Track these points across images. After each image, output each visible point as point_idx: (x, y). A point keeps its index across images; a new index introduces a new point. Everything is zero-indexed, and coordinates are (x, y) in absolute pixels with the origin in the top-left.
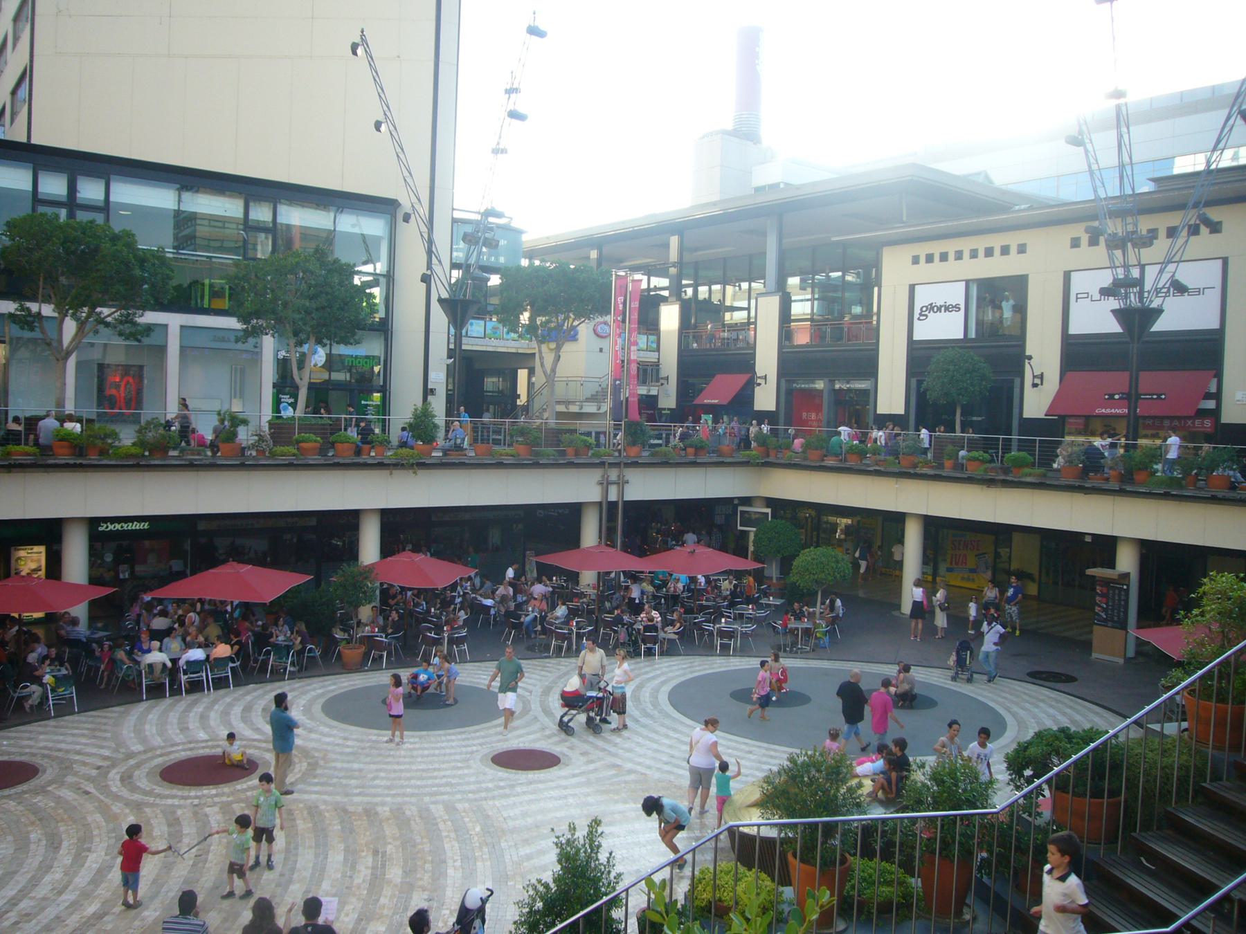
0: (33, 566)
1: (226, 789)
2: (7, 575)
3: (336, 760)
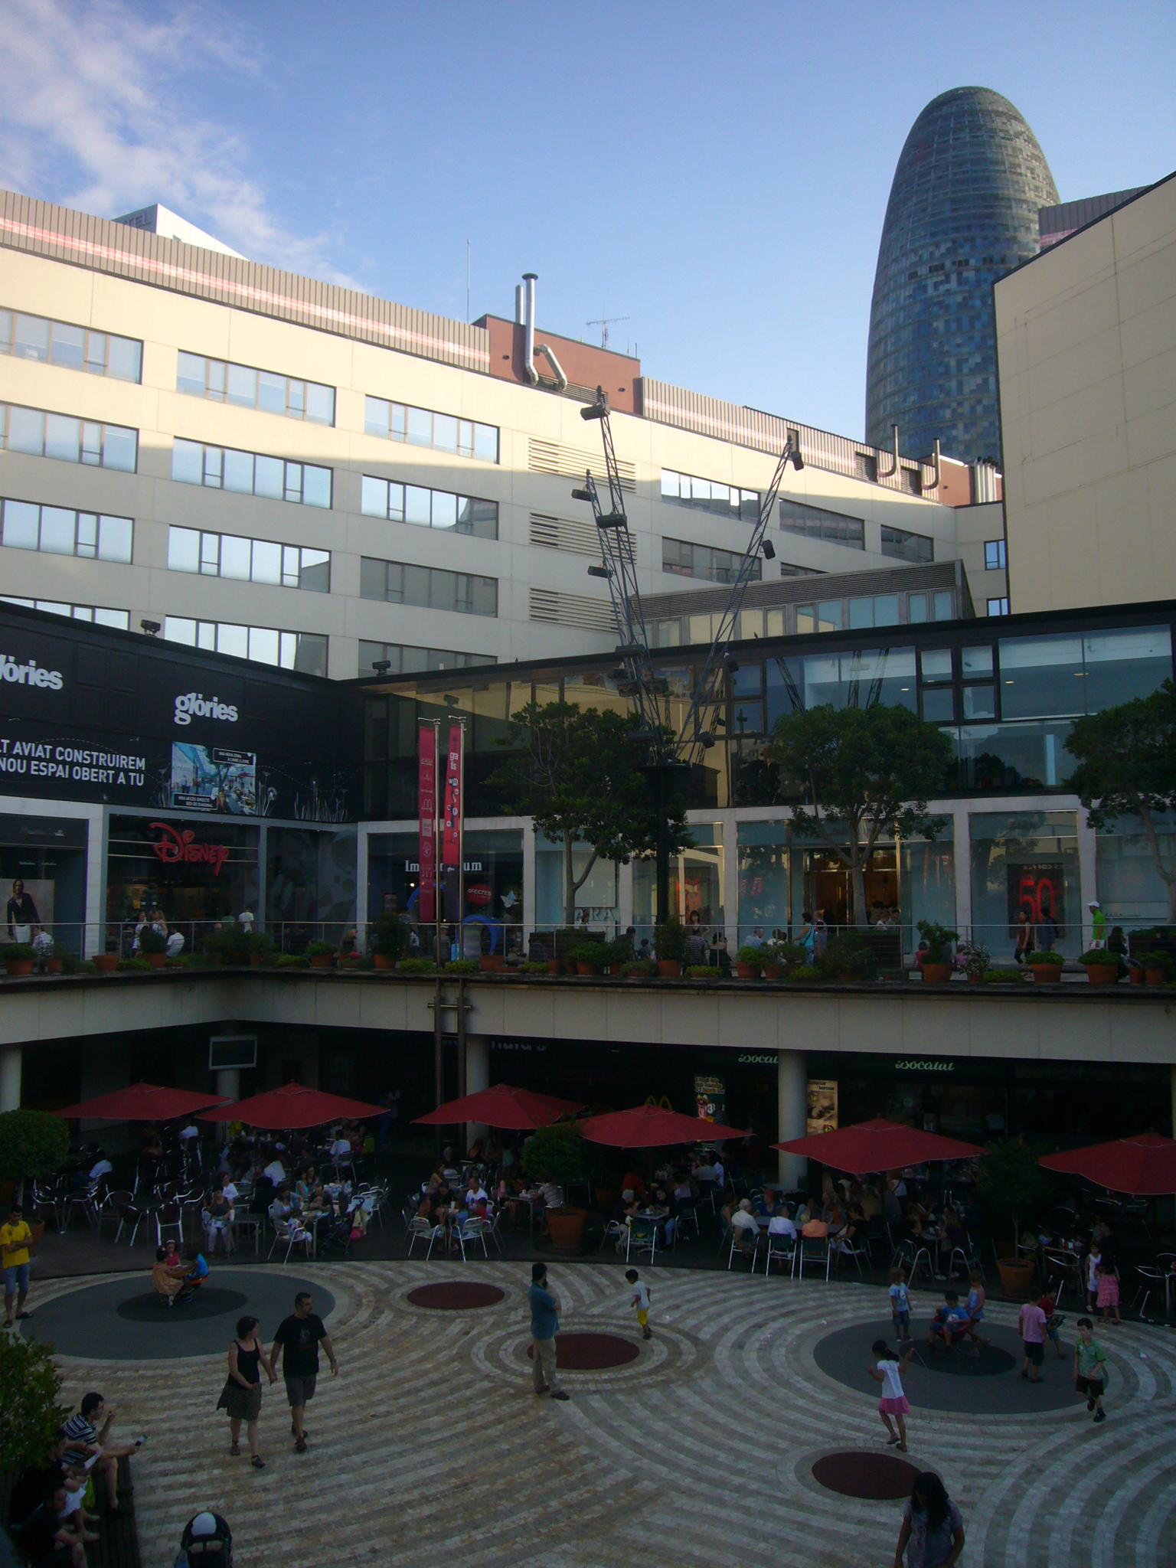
0: (826, 1103)
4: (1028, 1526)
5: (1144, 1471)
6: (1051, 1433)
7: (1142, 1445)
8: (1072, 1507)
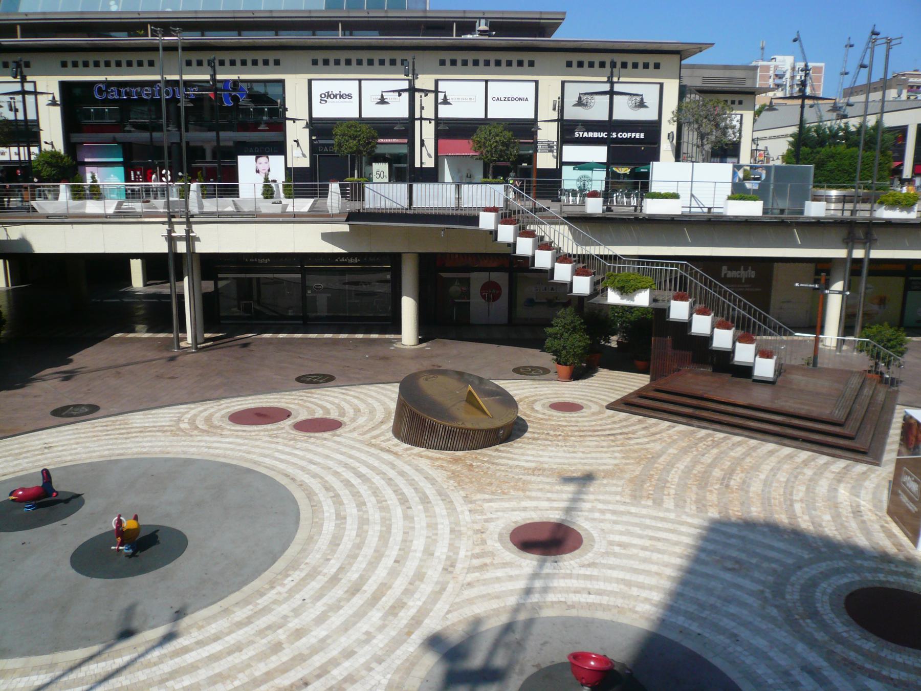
1: (869, 644)
2: (919, 125)
3: (751, 593)
4: (440, 526)
5: (375, 587)
6: (449, 612)
7: (376, 615)
8: (418, 544)
